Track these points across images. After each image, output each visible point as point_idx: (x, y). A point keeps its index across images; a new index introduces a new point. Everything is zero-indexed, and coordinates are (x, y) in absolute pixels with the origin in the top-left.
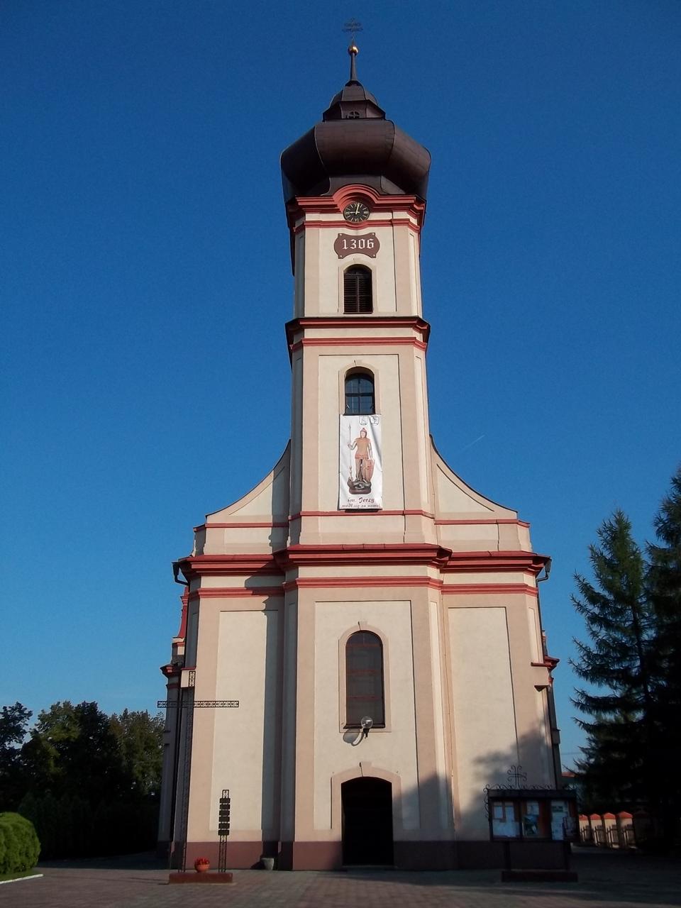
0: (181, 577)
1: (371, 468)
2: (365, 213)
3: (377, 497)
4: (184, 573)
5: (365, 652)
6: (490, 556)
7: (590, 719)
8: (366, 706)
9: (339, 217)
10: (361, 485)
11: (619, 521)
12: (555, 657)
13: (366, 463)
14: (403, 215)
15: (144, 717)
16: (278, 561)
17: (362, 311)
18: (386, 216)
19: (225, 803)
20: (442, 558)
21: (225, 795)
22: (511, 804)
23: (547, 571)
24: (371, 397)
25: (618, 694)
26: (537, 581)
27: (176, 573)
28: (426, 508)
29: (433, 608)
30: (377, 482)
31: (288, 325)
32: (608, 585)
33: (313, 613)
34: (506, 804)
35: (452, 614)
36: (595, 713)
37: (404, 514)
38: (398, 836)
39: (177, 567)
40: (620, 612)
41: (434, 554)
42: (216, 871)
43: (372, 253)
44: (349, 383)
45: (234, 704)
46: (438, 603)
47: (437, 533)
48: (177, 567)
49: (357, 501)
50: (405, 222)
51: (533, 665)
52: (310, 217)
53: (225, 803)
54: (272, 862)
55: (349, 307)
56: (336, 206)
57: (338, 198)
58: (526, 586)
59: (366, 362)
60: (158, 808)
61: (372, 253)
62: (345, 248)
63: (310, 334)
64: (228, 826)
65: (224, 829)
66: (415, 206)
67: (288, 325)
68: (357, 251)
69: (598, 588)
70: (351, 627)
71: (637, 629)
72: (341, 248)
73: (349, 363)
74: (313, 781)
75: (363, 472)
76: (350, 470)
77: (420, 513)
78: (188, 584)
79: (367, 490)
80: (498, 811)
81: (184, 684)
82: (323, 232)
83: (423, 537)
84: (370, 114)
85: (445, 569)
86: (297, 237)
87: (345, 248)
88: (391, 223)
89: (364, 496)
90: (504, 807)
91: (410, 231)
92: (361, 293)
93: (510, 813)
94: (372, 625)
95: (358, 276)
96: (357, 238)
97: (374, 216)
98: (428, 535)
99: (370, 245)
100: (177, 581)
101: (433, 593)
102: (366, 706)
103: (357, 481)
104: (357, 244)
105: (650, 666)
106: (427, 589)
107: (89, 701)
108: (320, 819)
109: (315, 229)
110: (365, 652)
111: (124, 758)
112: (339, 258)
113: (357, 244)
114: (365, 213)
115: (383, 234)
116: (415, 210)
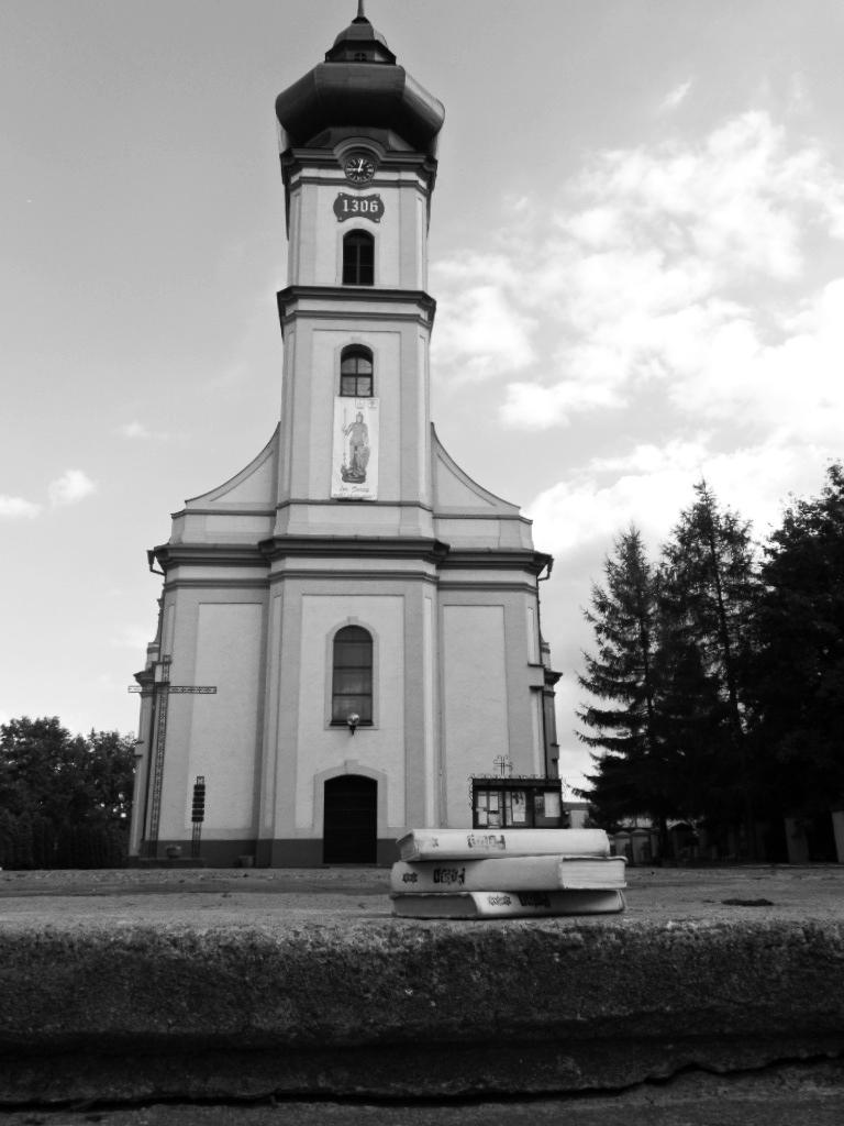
0: (157, 566)
1: (366, 454)
2: (370, 170)
3: (369, 489)
4: (160, 562)
5: (353, 645)
6: (489, 553)
7: (593, 732)
8: (352, 701)
9: (340, 174)
10: (355, 474)
11: (632, 530)
12: (555, 669)
13: (361, 450)
14: (412, 176)
15: (112, 740)
16: (264, 550)
17: (362, 283)
18: (393, 176)
19: (200, 791)
20: (439, 553)
21: (200, 781)
22: (496, 793)
23: (549, 570)
24: (368, 380)
25: (623, 708)
26: (538, 581)
27: (151, 562)
28: (425, 500)
29: (428, 606)
30: (372, 470)
31: (280, 295)
32: (618, 595)
33: (301, 607)
34: (491, 793)
35: (449, 612)
36: (596, 726)
37: (400, 505)
38: (381, 834)
39: (151, 555)
40: (630, 623)
41: (431, 548)
42: (189, 859)
43: (375, 217)
44: (346, 362)
45: (210, 690)
46: (434, 600)
47: (435, 528)
48: (151, 555)
49: (351, 490)
50: (413, 184)
51: (531, 666)
52: (307, 172)
53: (200, 791)
54: (250, 859)
55: (348, 275)
56: (336, 161)
57: (338, 153)
58: (526, 585)
59: (365, 339)
60: (129, 833)
61: (375, 217)
62: (346, 210)
63: (304, 305)
64: (202, 813)
65: (198, 816)
66: (425, 167)
67: (280, 295)
68: (359, 214)
69: (610, 597)
70: (340, 621)
71: (644, 641)
72: (341, 210)
73: (346, 339)
74: (295, 781)
75: (358, 460)
76: (342, 456)
77: (417, 505)
78: (165, 574)
79: (361, 479)
80: (482, 801)
81: (158, 678)
82: (322, 189)
83: (419, 529)
84: (377, 58)
85: (441, 566)
86: (293, 194)
87: (346, 210)
88: (398, 184)
89: (359, 486)
90: (488, 796)
91: (419, 195)
92: (361, 262)
93: (494, 803)
94: (363, 620)
95: (359, 243)
96: (360, 199)
97: (379, 176)
98: (424, 528)
99: (374, 207)
100: (152, 570)
101: (429, 589)
102: (352, 701)
103: (351, 469)
104: (359, 206)
105: (652, 678)
106: (379, 493)
107: (50, 716)
108: (304, 818)
109: (312, 186)
110: (353, 645)
111: (72, 967)
112: (339, 221)
113: (359, 206)
114: (370, 170)
115: (387, 195)
116: (425, 171)
